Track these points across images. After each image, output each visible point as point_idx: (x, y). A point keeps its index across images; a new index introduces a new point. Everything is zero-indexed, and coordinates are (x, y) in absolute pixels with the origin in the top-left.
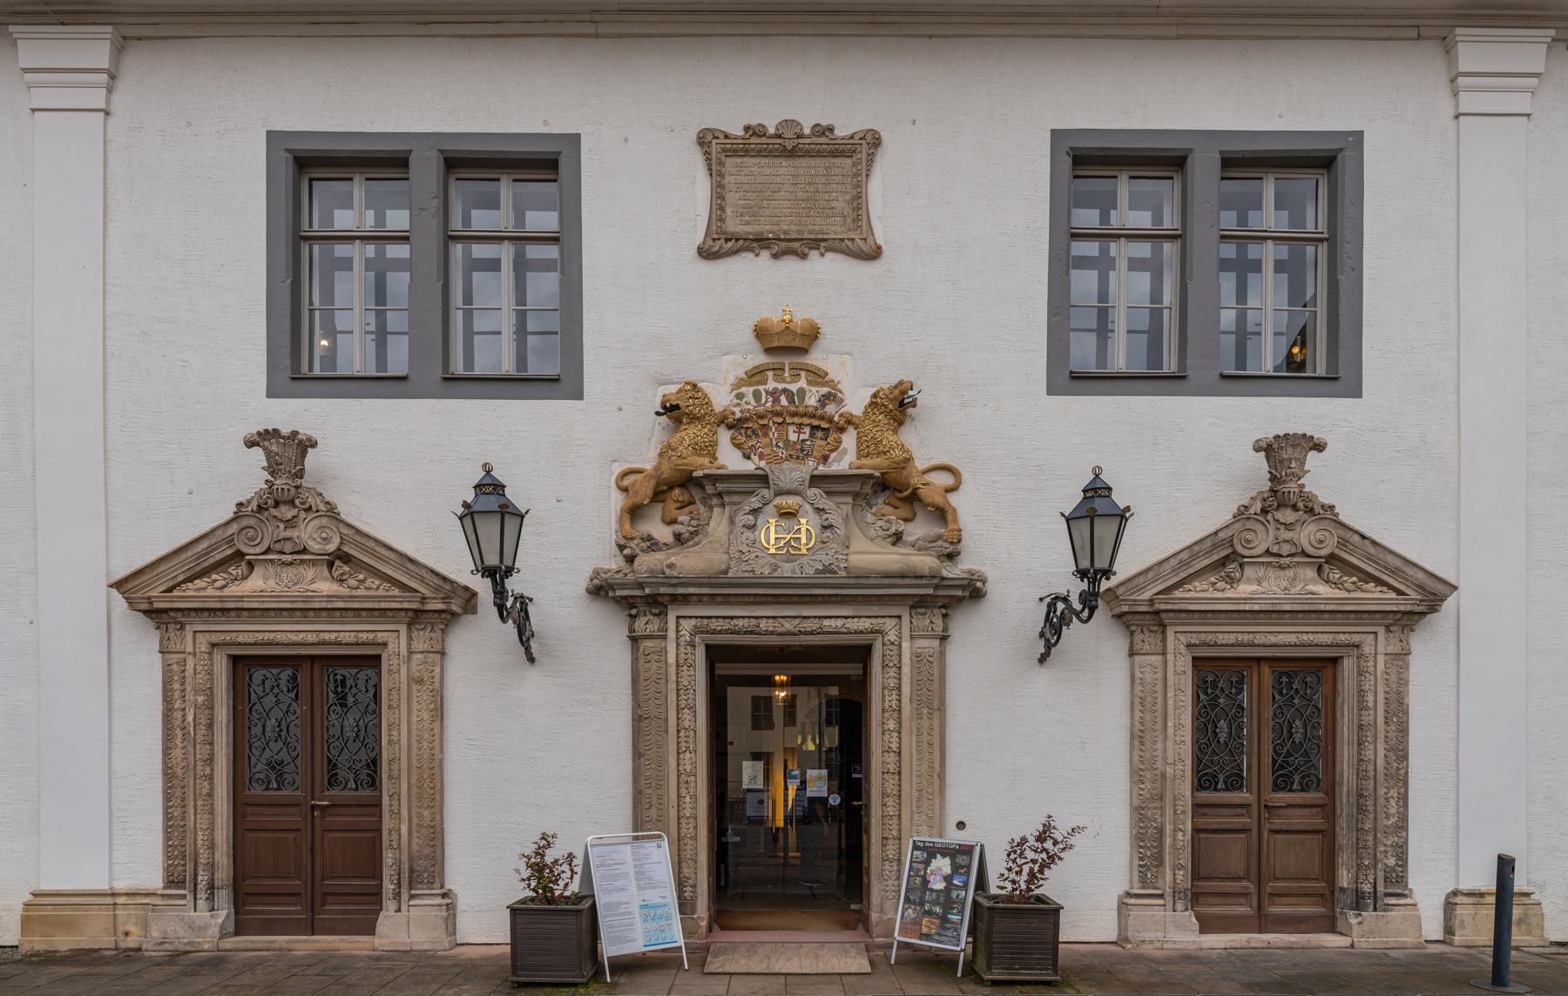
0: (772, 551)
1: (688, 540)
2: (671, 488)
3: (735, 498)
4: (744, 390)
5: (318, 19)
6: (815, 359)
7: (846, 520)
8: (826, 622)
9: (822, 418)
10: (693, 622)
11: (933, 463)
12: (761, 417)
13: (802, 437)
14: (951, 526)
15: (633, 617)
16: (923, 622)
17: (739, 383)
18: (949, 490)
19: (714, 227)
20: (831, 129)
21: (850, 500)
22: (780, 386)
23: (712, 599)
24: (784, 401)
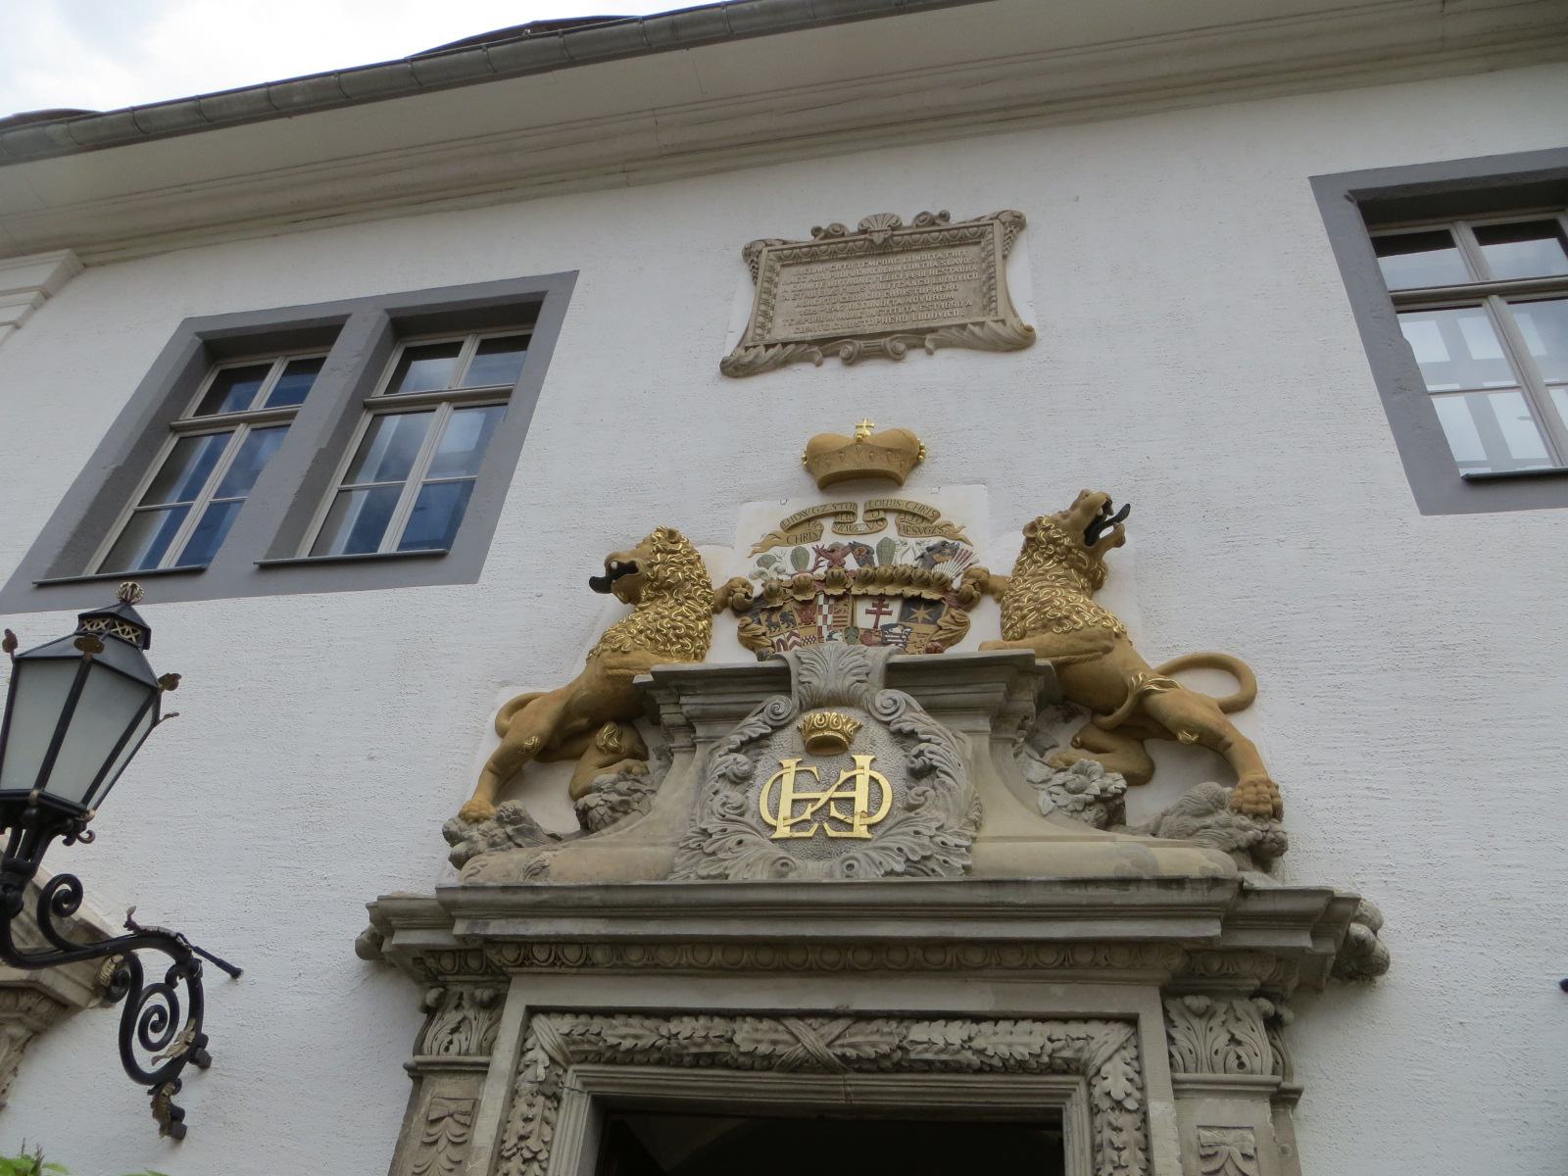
0: (783, 831)
2: (596, 726)
3: (719, 729)
4: (774, 551)
5: (299, 216)
6: (914, 493)
7: (975, 764)
8: (919, 1032)
9: (926, 583)
10: (565, 1024)
11: (1178, 655)
13: (884, 620)
14: (1246, 777)
15: (431, 1012)
16: (1206, 1040)
17: (772, 540)
18: (1232, 708)
19: (750, 334)
20: (944, 216)
21: (984, 724)
22: (845, 541)
24: (851, 563)
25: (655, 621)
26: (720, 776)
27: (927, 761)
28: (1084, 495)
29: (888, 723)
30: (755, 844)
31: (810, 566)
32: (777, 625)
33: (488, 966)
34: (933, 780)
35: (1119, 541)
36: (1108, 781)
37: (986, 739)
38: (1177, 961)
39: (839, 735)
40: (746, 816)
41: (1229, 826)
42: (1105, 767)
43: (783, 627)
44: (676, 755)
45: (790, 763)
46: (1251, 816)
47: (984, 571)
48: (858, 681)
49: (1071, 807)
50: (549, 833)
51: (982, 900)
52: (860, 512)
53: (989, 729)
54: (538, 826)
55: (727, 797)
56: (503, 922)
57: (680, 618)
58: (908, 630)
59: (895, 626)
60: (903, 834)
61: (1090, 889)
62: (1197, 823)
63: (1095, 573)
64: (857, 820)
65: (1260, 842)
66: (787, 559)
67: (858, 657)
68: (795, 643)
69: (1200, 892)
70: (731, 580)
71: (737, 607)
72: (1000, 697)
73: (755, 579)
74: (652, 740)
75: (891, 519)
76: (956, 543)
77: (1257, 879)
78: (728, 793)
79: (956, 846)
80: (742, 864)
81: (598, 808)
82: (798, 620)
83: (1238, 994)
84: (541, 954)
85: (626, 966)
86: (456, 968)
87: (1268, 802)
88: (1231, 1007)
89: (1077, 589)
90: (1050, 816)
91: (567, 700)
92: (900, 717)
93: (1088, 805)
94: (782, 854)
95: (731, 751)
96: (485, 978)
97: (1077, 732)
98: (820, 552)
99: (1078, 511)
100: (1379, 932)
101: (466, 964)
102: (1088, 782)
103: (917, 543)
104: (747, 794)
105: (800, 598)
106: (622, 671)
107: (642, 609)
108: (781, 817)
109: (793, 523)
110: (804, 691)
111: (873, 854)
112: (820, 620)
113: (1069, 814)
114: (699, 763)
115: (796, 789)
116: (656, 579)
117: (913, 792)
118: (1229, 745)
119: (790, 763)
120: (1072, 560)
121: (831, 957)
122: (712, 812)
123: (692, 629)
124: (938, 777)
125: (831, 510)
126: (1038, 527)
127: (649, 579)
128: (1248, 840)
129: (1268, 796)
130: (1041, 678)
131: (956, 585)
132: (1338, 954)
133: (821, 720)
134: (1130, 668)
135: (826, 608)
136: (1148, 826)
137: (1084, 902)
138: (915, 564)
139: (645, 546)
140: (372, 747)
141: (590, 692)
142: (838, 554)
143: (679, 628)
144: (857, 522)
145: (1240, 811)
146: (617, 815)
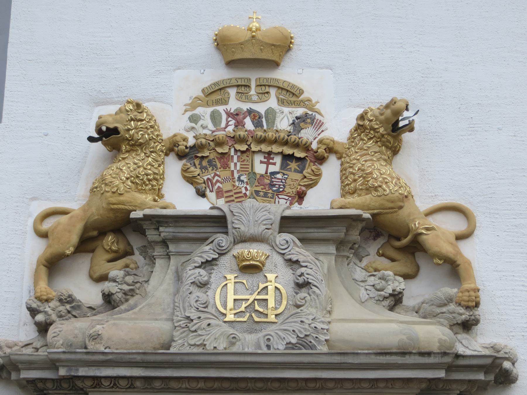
0: (230, 317)
2: (103, 233)
3: (184, 247)
4: (199, 111)
6: (287, 73)
9: (296, 145)
12: (219, 143)
13: (272, 169)
18: (460, 237)
21: (332, 249)
22: (245, 107)
24: (249, 124)
25: (135, 170)
26: (191, 283)
27: (306, 279)
28: (393, 102)
29: (284, 254)
30: (217, 325)
31: (223, 125)
32: (206, 168)
34: (309, 290)
36: (397, 284)
37: (334, 258)
43: (210, 169)
44: (157, 260)
46: (465, 308)
47: (331, 141)
48: (266, 229)
49: (377, 298)
50: (88, 306)
51: (336, 361)
52: (253, 85)
55: (198, 297)
56: (86, 369)
57: (149, 167)
58: (286, 176)
59: (278, 173)
60: (295, 322)
61: (387, 356)
62: (439, 310)
63: (396, 147)
64: (269, 312)
65: (468, 321)
67: (265, 213)
68: (217, 181)
69: (437, 358)
70: (175, 136)
72: (342, 235)
73: (188, 131)
75: (273, 92)
76: (314, 114)
80: (212, 338)
81: (117, 294)
84: (106, 383)
85: (153, 388)
87: (473, 301)
89: (385, 160)
90: (366, 303)
91: (85, 221)
92: (290, 251)
93: (385, 298)
94: (232, 331)
95: (196, 267)
96: (71, 392)
97: (380, 246)
98: (229, 114)
99: (388, 112)
100: (516, 364)
101: (61, 385)
102: (386, 285)
103: (290, 113)
104: (207, 293)
105: (220, 150)
106: (120, 206)
107: (124, 159)
108: (228, 308)
109: (212, 90)
111: (280, 333)
113: (375, 302)
115: (235, 292)
116: (132, 140)
117: (298, 296)
118: (458, 265)
119: (231, 277)
120: (384, 142)
122: (191, 306)
123: (157, 174)
124: (311, 288)
126: (365, 117)
127: (127, 139)
128: (462, 320)
129: (474, 298)
131: (314, 146)
133: (248, 254)
134: (411, 218)
135: (235, 157)
136: (414, 307)
137: (384, 363)
138: (289, 128)
141: (100, 217)
142: (241, 116)
143: (150, 175)
145: (460, 305)
146: (128, 297)
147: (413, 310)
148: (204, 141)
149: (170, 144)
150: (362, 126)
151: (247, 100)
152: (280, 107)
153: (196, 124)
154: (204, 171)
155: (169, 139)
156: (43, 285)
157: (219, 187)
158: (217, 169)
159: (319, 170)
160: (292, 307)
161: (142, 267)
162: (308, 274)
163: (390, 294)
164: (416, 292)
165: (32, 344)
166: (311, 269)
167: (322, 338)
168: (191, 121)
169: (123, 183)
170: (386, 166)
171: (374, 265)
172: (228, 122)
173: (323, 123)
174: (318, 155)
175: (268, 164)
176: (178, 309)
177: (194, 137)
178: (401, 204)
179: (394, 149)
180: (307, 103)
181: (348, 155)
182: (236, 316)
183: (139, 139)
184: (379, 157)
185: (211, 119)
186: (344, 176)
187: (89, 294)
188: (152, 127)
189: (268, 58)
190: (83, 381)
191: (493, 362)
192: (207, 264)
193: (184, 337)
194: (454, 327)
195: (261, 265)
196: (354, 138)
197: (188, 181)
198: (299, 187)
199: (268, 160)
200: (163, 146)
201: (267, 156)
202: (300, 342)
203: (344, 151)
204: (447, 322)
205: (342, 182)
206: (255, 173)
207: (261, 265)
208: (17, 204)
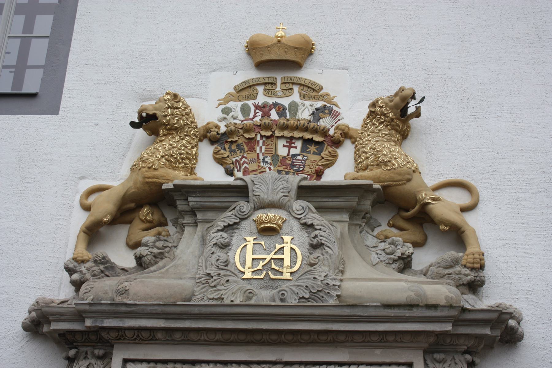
0: (248, 275)
1: (150, 264)
2: (140, 206)
3: (210, 215)
4: (231, 104)
6: (308, 74)
9: (315, 131)
12: (247, 130)
13: (293, 151)
18: (464, 210)
22: (271, 101)
23: (170, 337)
24: (274, 115)
25: (170, 149)
26: (214, 244)
27: (319, 241)
28: (402, 90)
29: (299, 219)
30: (235, 282)
31: (251, 116)
32: (234, 151)
33: (100, 339)
35: (417, 114)
36: (406, 248)
37: (347, 225)
38: (432, 340)
39: (275, 226)
40: (229, 266)
41: (460, 274)
42: (403, 239)
44: (186, 227)
45: (250, 239)
47: (347, 127)
48: (284, 196)
49: (387, 261)
51: (346, 314)
52: (279, 83)
53: (348, 220)
54: (115, 264)
57: (183, 148)
58: (306, 158)
59: (299, 155)
60: (308, 279)
61: (395, 309)
63: (404, 131)
64: (285, 270)
65: (473, 282)
66: (238, 110)
68: (244, 162)
70: (208, 124)
71: (212, 139)
72: (354, 204)
74: (169, 216)
75: (296, 88)
76: (332, 106)
77: (469, 301)
78: (219, 254)
79: (333, 285)
80: (230, 292)
81: (148, 256)
82: (246, 149)
83: (457, 352)
85: (173, 340)
86: (83, 340)
88: (454, 359)
89: (394, 141)
90: (376, 266)
92: (305, 216)
93: (395, 261)
95: (219, 231)
97: (390, 218)
98: (257, 107)
99: (397, 99)
104: (228, 254)
105: (247, 136)
106: (154, 180)
107: (161, 141)
108: (247, 267)
109: (243, 87)
110: (256, 200)
111: (294, 289)
112: (258, 149)
114: (200, 233)
116: (168, 124)
117: (312, 256)
118: (463, 232)
119: (250, 239)
120: (393, 125)
121: (274, 337)
122: (212, 264)
125: (262, 81)
126: (377, 105)
127: (164, 124)
128: (468, 281)
129: (479, 260)
130: (375, 194)
131: (331, 132)
132: (501, 336)
133: (266, 218)
135: (261, 142)
136: (422, 271)
137: (392, 315)
139: (161, 104)
140: (11, 213)
141: (136, 190)
142: (267, 109)
143: (183, 154)
144: (276, 90)
146: (158, 260)
147: (421, 273)
148: (233, 128)
149: (204, 131)
150: (374, 112)
151: (272, 96)
152: (301, 101)
153: (228, 115)
154: (233, 154)
155: (203, 127)
156: (82, 247)
157: (246, 167)
158: (245, 152)
159: (336, 152)
160: (307, 266)
161: (173, 235)
162: (321, 236)
163: (399, 257)
164: (423, 258)
165: (67, 301)
166: (325, 231)
167: (334, 293)
168: (223, 113)
169: (158, 160)
170: (395, 145)
171: (385, 233)
172: (255, 114)
173: (339, 113)
174: (335, 139)
175: (290, 147)
176: (201, 268)
177: (225, 126)
178: (409, 177)
179: (402, 133)
180: (325, 97)
181: (361, 139)
182: (254, 274)
183: (175, 124)
184: (389, 138)
185: (241, 111)
186: (357, 155)
187: (123, 258)
188: (187, 114)
189: (291, 59)
190: (108, 333)
191: (499, 317)
192: (229, 228)
193: (204, 292)
194: (460, 287)
195: (278, 228)
196: (367, 124)
197: (218, 163)
198: (317, 167)
199: (290, 145)
200: (197, 132)
201: (289, 140)
202: (313, 297)
203: (358, 136)
204: (453, 282)
205: (356, 161)
206: (278, 155)
207: (278, 228)
208: (67, 182)
